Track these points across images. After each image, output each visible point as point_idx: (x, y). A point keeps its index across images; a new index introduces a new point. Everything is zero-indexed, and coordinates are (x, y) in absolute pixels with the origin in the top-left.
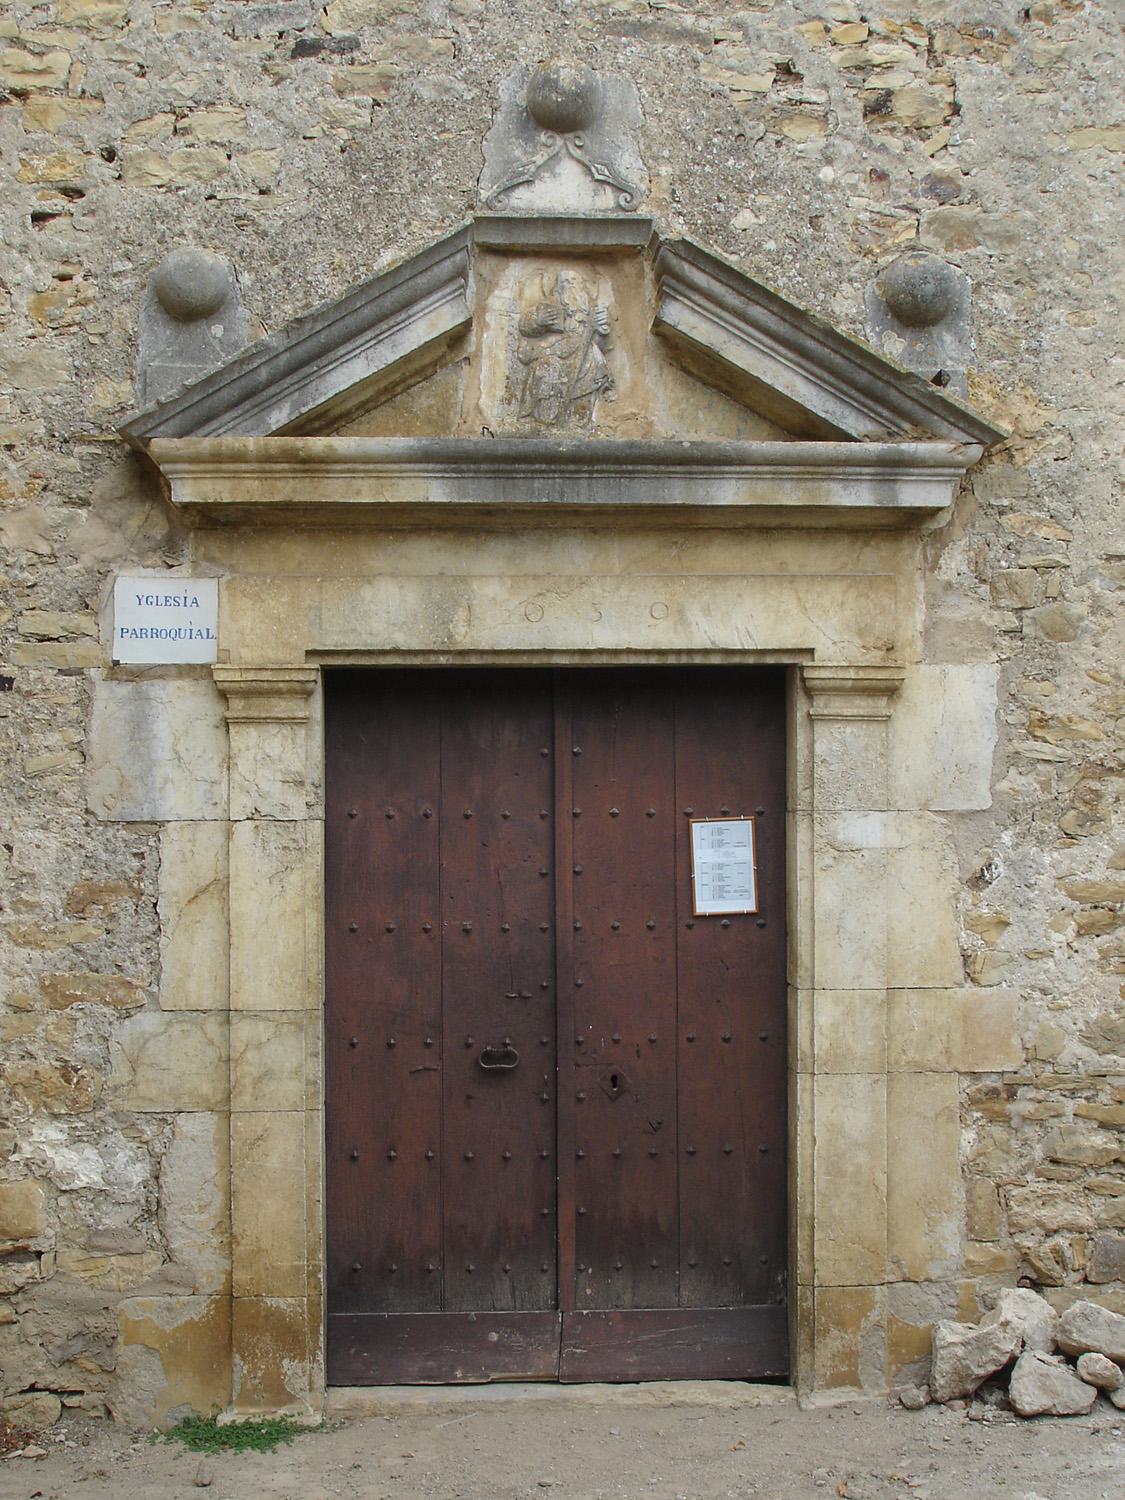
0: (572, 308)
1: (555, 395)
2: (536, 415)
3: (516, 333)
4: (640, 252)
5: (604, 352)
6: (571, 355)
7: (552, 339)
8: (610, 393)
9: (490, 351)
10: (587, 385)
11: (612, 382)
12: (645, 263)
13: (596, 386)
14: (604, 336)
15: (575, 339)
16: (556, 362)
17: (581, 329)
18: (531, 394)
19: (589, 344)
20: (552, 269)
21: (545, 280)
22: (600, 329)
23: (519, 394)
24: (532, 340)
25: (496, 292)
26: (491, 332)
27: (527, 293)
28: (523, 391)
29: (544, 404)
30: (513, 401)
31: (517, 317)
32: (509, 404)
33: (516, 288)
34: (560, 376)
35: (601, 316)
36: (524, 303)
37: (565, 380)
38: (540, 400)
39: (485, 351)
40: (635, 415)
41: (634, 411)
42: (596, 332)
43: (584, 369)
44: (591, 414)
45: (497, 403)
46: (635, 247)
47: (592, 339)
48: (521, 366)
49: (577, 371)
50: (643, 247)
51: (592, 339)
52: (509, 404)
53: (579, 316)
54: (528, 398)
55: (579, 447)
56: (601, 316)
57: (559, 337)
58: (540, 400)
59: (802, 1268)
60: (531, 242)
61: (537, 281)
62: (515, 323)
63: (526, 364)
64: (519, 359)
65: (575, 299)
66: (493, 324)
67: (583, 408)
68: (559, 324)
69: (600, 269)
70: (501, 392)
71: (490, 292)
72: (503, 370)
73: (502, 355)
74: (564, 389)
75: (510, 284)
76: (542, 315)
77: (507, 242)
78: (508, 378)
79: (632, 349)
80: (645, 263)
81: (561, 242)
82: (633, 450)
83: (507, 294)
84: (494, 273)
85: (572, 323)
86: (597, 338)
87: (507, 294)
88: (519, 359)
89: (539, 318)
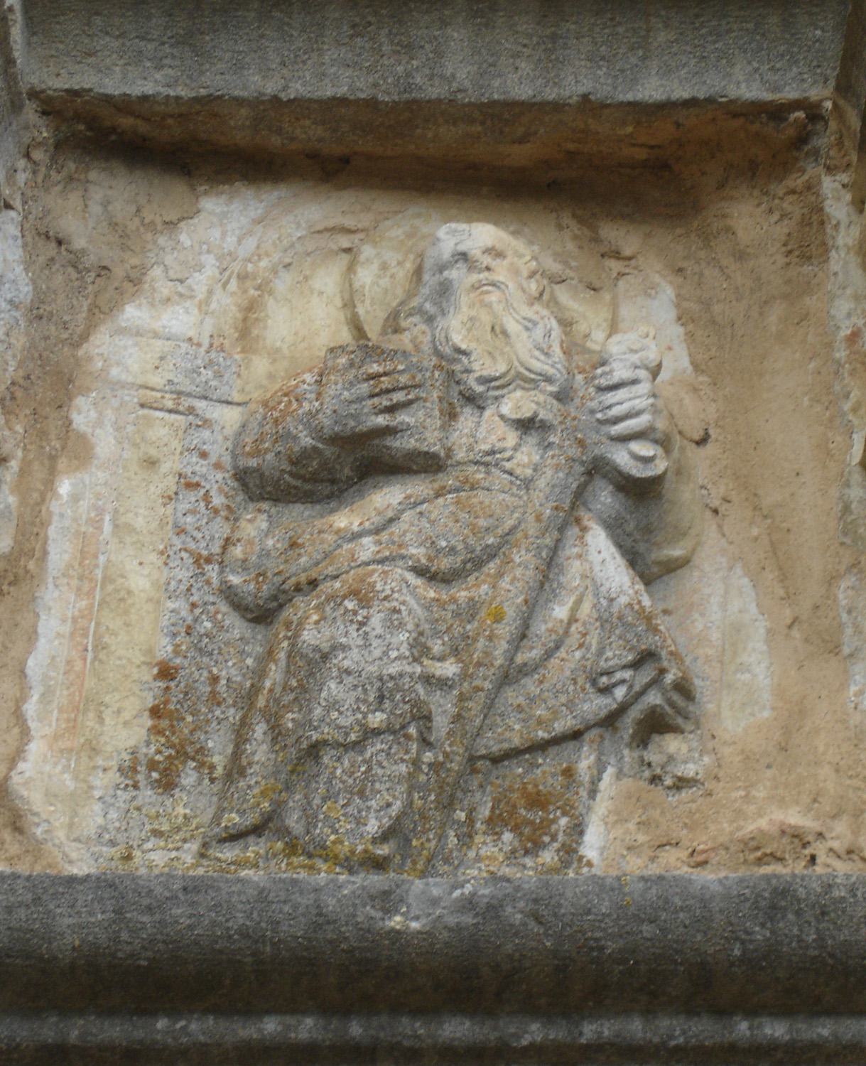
0: (483, 365)
1: (394, 730)
2: (293, 821)
3: (217, 483)
4: (801, 139)
5: (650, 569)
6: (477, 563)
7: (388, 497)
8: (672, 744)
9: (86, 552)
10: (557, 696)
11: (684, 689)
12: (829, 184)
13: (596, 706)
14: (641, 491)
15: (497, 499)
16: (407, 593)
17: (526, 456)
18: (276, 733)
19: (568, 517)
20: (396, 230)
21: (365, 276)
22: (621, 458)
23: (218, 747)
24: (296, 513)
25: (132, 313)
26: (96, 476)
27: (280, 326)
28: (241, 735)
29: (337, 767)
30: (189, 778)
31: (230, 418)
32: (167, 784)
33: (227, 303)
34: (420, 650)
35: (622, 401)
36: (260, 365)
37: (449, 669)
38: (314, 750)
39: (60, 552)
40: (798, 838)
41: (794, 818)
42: (597, 469)
43: (540, 628)
44: (578, 830)
45: (103, 782)
46: (777, 112)
47: (579, 497)
48: (237, 627)
49: (505, 631)
50: (814, 113)
51: (579, 497)
52: (167, 784)
53: (516, 403)
54: (260, 750)
55: (493, 909)
56: (622, 401)
57: (418, 487)
58: (314, 750)
59: (478, 220)
60: (297, 89)
61: (328, 280)
62: (219, 449)
63: (262, 614)
64: (229, 594)
65: (499, 331)
66: (105, 444)
67: (538, 801)
68: (420, 428)
69: (626, 238)
70: (126, 731)
71: (100, 312)
72: (142, 636)
73: (141, 576)
74: (442, 708)
75: (200, 282)
76: (336, 390)
77: (182, 92)
78: (166, 672)
79: (776, 562)
80: (829, 184)
81: (435, 91)
82: (788, 925)
83: (179, 320)
84: (123, 238)
85: (486, 430)
86: (605, 497)
87: (179, 320)
88: (229, 594)
89: (340, 402)
